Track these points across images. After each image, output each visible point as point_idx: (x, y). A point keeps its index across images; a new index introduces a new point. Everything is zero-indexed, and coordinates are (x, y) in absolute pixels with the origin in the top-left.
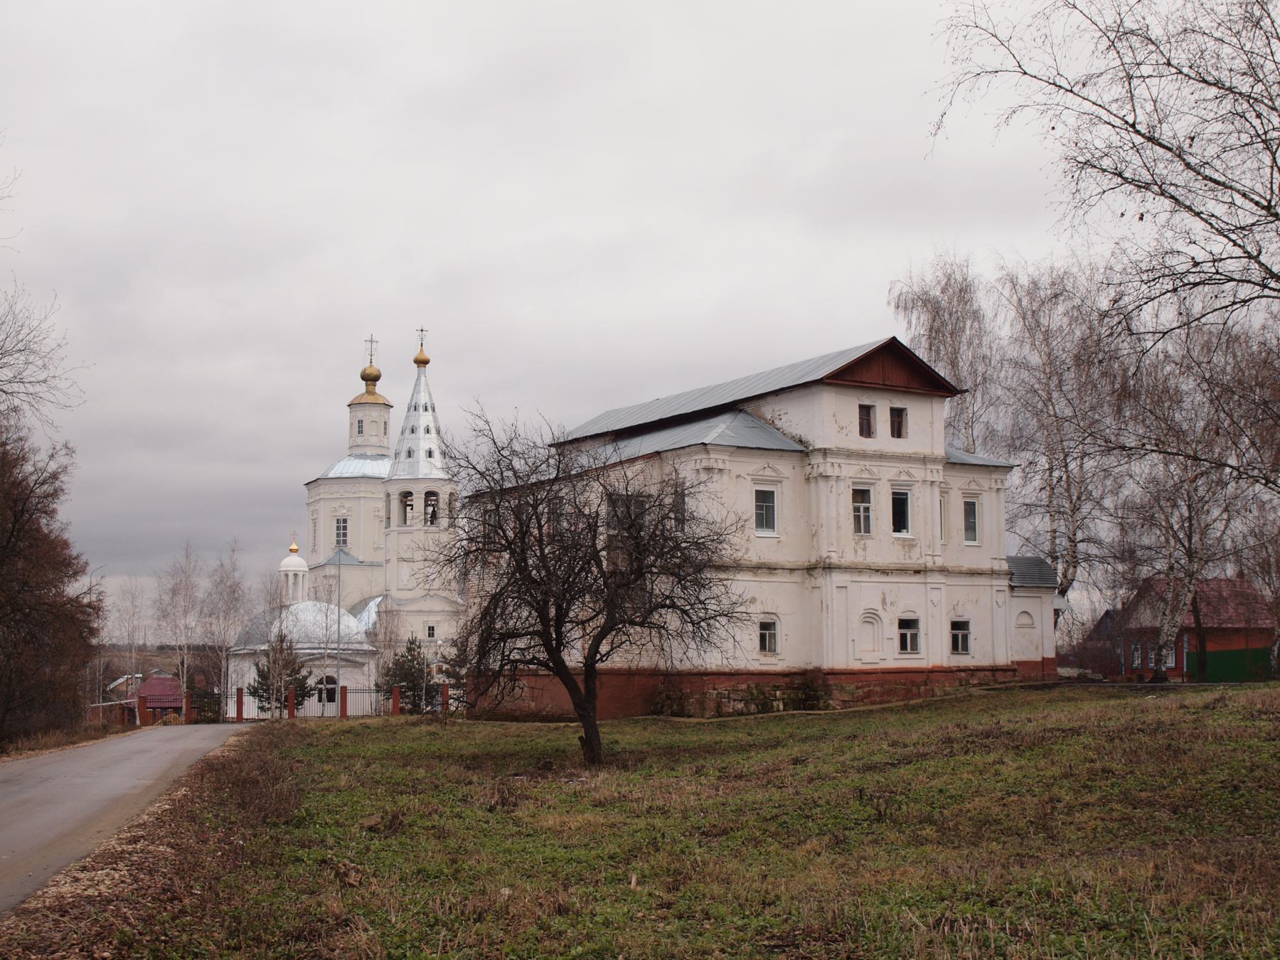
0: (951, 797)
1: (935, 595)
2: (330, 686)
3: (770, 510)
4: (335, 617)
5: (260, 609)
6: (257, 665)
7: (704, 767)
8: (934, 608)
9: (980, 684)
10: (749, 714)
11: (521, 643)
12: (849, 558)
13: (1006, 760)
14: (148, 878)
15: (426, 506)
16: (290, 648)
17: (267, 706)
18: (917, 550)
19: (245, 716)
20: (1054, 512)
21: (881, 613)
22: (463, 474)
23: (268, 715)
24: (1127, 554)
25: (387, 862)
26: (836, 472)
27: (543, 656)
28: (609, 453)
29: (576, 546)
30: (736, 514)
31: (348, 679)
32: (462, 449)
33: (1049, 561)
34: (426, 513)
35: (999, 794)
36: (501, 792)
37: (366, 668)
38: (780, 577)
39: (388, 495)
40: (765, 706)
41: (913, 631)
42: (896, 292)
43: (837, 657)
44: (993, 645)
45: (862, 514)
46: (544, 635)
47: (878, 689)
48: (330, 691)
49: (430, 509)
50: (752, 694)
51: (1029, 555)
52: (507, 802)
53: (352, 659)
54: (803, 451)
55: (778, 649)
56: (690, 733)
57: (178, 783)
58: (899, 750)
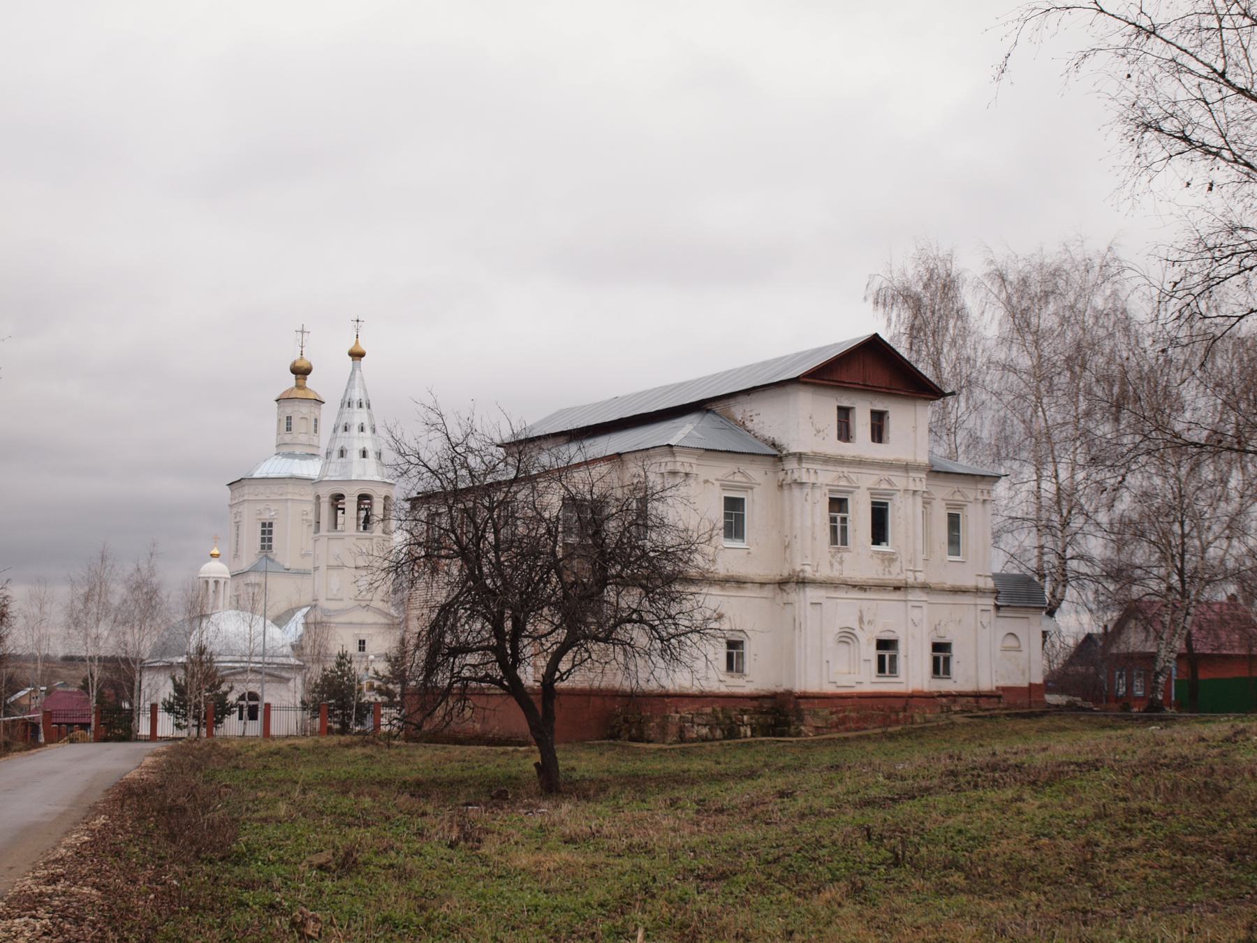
0: (974, 839)
1: (916, 615)
2: (252, 703)
3: (740, 519)
4: (260, 628)
5: (180, 617)
6: (173, 679)
7: (679, 799)
8: (914, 628)
9: (963, 711)
10: (714, 739)
11: (472, 659)
12: (824, 572)
13: (1025, 797)
14: (74, 928)
15: (359, 509)
16: (211, 661)
17: (184, 723)
18: (898, 564)
19: (159, 734)
20: (1043, 527)
21: (857, 632)
22: (413, 472)
23: (184, 733)
24: (1120, 573)
25: (346, 908)
26: (812, 479)
27: (497, 673)
28: (573, 452)
29: (535, 552)
30: (710, 521)
31: (272, 695)
32: (413, 444)
33: (1036, 578)
34: (358, 519)
35: (1028, 836)
36: (462, 827)
37: (291, 684)
38: (750, 592)
39: (318, 497)
40: (731, 732)
41: (892, 652)
42: (875, 287)
43: (810, 681)
44: (977, 670)
45: (839, 525)
46: (498, 650)
47: (853, 714)
48: (253, 709)
49: (363, 514)
50: (717, 718)
51: (1016, 572)
52: (470, 837)
53: (276, 674)
54: (776, 456)
55: (747, 670)
56: (651, 760)
57: (94, 810)
58: (898, 784)
